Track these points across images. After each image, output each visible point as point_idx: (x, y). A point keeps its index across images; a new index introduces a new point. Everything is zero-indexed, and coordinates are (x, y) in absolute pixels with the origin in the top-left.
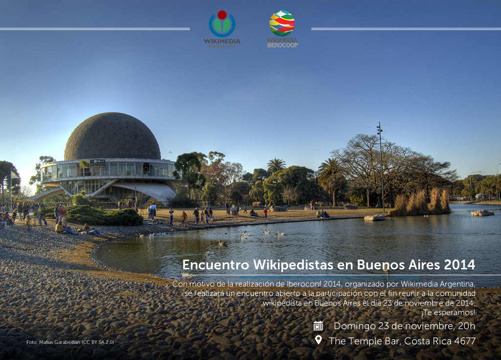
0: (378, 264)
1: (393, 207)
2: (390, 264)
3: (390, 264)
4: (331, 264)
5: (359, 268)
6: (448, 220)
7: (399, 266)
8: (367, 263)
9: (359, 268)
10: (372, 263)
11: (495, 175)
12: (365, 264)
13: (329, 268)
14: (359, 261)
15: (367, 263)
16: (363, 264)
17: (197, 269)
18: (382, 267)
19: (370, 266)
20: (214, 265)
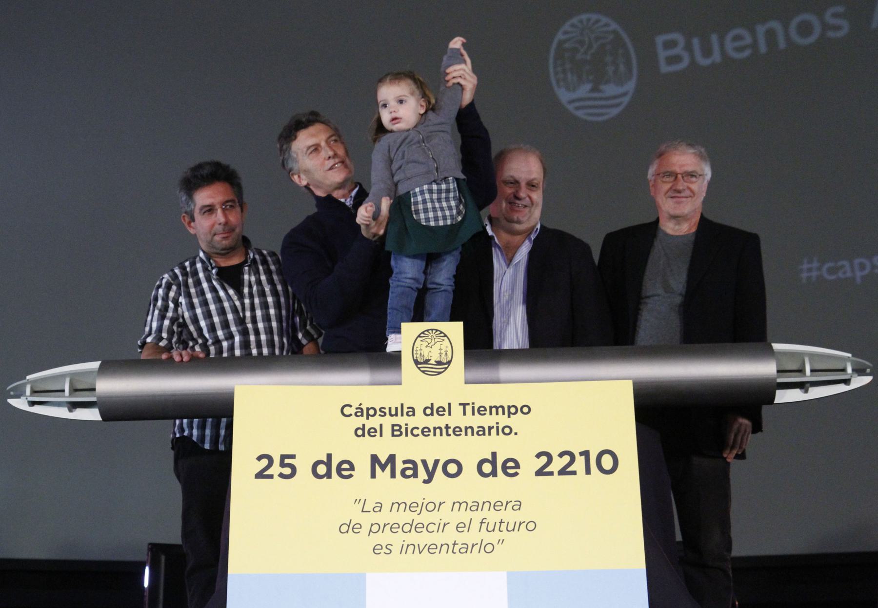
0: (738, 38)
1: (537, 205)
2: (786, 27)
3: (786, 27)
4: (836, 15)
5: (665, 68)
6: (530, 211)
7: (825, 27)
8: (696, 42)
9: (665, 68)
10: (714, 38)
11: (752, 442)
12: (689, 48)
13: (831, 34)
14: (660, 40)
15: (696, 42)
16: (678, 50)
17: (782, 44)
18: (754, 45)
19: (707, 52)
20: (722, 45)
